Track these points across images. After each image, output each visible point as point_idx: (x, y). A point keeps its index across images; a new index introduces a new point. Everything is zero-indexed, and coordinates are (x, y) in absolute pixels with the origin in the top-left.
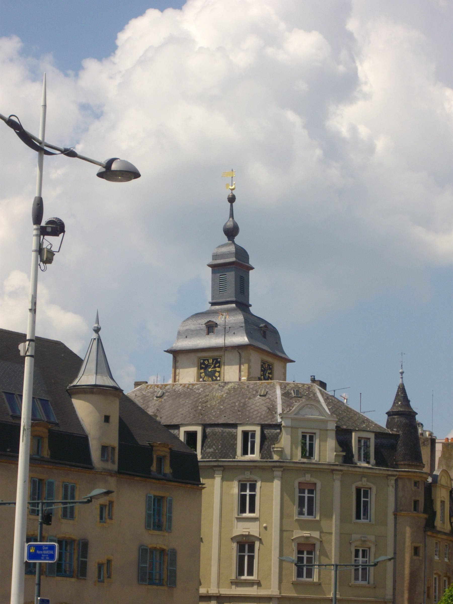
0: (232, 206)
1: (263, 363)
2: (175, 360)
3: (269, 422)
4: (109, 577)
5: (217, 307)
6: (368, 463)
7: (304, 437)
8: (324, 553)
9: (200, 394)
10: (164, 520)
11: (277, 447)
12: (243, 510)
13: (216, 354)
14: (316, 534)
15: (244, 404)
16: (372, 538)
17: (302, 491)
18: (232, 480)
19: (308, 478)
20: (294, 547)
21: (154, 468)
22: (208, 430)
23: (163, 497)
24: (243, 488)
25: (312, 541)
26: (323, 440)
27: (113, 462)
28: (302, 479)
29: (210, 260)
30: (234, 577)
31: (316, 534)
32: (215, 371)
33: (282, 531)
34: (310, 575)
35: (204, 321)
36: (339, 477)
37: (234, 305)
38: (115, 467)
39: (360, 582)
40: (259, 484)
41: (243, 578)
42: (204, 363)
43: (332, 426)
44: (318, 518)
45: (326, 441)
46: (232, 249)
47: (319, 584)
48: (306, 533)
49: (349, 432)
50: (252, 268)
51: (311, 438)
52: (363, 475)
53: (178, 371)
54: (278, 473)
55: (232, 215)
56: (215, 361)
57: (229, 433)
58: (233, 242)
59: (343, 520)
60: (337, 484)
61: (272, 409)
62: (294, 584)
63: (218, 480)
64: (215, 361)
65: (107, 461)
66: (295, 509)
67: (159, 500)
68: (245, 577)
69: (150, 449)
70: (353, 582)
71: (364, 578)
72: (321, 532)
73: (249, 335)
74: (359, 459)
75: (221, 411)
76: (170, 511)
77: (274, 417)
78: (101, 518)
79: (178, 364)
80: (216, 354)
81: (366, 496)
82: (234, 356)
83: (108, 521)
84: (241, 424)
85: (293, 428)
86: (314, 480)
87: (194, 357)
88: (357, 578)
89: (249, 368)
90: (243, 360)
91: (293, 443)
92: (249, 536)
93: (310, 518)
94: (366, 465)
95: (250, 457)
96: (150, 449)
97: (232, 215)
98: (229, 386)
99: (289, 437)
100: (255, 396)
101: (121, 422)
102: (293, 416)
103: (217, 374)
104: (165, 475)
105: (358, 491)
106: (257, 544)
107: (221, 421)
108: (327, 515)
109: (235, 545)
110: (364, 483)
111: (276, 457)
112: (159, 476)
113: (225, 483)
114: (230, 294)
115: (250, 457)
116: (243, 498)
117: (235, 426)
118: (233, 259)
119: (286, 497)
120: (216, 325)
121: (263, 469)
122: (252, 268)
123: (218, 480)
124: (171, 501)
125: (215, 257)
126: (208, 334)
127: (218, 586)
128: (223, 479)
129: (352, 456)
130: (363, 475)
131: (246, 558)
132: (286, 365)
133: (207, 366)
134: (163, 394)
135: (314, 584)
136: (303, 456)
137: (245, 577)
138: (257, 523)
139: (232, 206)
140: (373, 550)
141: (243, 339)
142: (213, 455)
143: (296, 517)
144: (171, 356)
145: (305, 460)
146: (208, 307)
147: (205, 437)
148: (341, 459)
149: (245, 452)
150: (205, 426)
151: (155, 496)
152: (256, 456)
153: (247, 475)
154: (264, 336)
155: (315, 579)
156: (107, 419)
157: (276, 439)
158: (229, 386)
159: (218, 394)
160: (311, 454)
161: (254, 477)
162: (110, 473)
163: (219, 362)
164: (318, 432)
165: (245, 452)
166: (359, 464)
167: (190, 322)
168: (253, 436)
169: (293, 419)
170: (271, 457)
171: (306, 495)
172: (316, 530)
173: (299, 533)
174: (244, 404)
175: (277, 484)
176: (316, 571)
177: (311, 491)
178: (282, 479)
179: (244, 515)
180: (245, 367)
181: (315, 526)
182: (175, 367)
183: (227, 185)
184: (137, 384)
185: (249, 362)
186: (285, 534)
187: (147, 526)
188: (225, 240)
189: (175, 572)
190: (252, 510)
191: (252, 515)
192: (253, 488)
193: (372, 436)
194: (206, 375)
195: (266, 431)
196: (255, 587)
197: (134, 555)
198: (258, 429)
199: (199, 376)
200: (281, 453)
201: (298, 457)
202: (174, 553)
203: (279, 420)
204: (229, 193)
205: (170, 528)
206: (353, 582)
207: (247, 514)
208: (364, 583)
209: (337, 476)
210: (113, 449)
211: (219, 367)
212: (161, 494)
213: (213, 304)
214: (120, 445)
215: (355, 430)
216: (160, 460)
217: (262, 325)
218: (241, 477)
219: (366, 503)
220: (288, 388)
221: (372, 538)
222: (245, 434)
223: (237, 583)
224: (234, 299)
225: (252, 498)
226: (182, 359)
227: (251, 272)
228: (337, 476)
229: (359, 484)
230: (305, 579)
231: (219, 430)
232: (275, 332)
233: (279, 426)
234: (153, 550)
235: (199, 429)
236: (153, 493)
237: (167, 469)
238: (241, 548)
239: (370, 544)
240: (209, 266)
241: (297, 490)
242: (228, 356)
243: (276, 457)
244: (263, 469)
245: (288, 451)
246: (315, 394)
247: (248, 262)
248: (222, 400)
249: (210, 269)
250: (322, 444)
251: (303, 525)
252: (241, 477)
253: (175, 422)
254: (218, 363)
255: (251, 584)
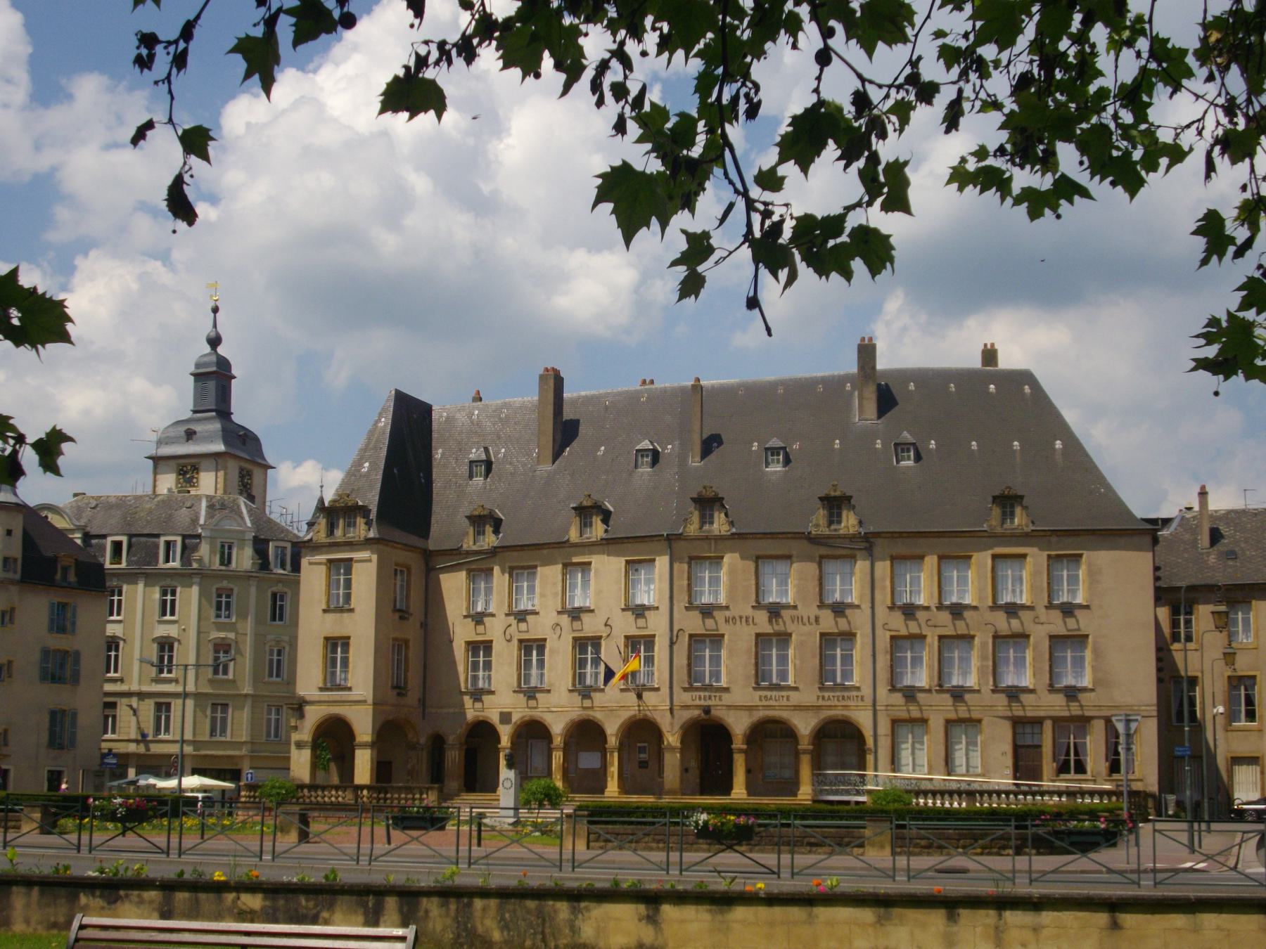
0: (215, 317)
1: (242, 469)
2: (155, 467)
3: (190, 532)
4: (10, 676)
5: (199, 415)
6: (284, 569)
7: (223, 546)
8: (239, 652)
9: (131, 506)
10: (68, 624)
11: (196, 555)
12: (164, 614)
13: (193, 461)
14: (232, 635)
15: (170, 515)
16: (286, 638)
17: (219, 596)
18: (154, 586)
19: (225, 584)
20: (211, 647)
21: (58, 576)
22: (134, 540)
23: (67, 604)
24: (164, 593)
25: (228, 642)
26: (241, 548)
27: (15, 572)
28: (219, 585)
29: (192, 369)
30: (154, 675)
31: (232, 635)
32: (193, 477)
33: (199, 633)
34: (225, 672)
35: (183, 429)
36: (255, 583)
37: (214, 414)
38: (18, 576)
39: (274, 679)
40: (178, 590)
41: (163, 675)
42: (182, 470)
43: (250, 535)
44: (234, 620)
45: (243, 549)
46: (214, 358)
47: (234, 681)
48: (222, 635)
49: (267, 541)
50: (235, 377)
51: (230, 548)
52: (279, 581)
53: (158, 477)
54: (196, 580)
55: (215, 326)
56: (1214, 330)
57: (153, 543)
58: (216, 351)
59: (258, 622)
60: (253, 590)
61: (195, 521)
62: (211, 682)
63: (141, 586)
64: (1214, 330)
65: (8, 571)
66: (213, 612)
67: (63, 607)
68: (165, 675)
69: (55, 560)
70: (267, 679)
71: (278, 676)
72: (237, 633)
73: (226, 443)
74: (276, 566)
75: (148, 522)
76: (74, 615)
77: (195, 527)
78: (3, 623)
79: (158, 470)
80: (193, 461)
81: (282, 600)
82: (211, 463)
83: (9, 625)
84: (164, 535)
85: (212, 539)
86: (231, 586)
87: (173, 463)
88: (271, 675)
89: (226, 474)
90: (219, 467)
91: (212, 552)
92: (168, 637)
93: (227, 620)
94: (282, 572)
95: (171, 564)
96: (55, 560)
97: (215, 326)
98: (160, 497)
99: (208, 546)
100: (181, 508)
101: (26, 535)
102: (211, 527)
103: (195, 480)
104: (70, 583)
105: (274, 595)
106: (176, 645)
107: (146, 532)
108: (243, 616)
109: (155, 646)
110: (279, 588)
111: (195, 565)
112: (65, 584)
113: (147, 589)
114: (211, 402)
115: (171, 564)
116: (164, 603)
117: (158, 536)
118: (214, 369)
119: (204, 602)
120: (195, 433)
121: (182, 575)
122: (235, 377)
123: (141, 586)
124: (75, 609)
125: (198, 366)
126: (188, 440)
127: (140, 683)
128: (146, 585)
129: (269, 563)
130: (279, 581)
131: (166, 657)
132: (266, 474)
133: (185, 473)
134: (97, 505)
135: (228, 681)
136: (222, 563)
137: (165, 675)
138: (177, 625)
139: (215, 317)
140: (287, 649)
141: (221, 447)
142: (137, 563)
143: (213, 620)
144: (151, 462)
145: (223, 568)
146: (188, 415)
147: (130, 546)
148: (257, 567)
149: (167, 560)
150: (131, 536)
151: (59, 604)
152: (175, 564)
153: (168, 582)
154: (244, 443)
155: (231, 676)
156: (9, 533)
157: (195, 548)
158: (160, 497)
159: (148, 506)
160: (229, 562)
161: (174, 583)
162: (12, 582)
163: (197, 469)
164: (235, 542)
165: (167, 560)
166: (275, 571)
167: (171, 429)
168: (175, 546)
169: (212, 530)
170: (191, 565)
171: (224, 599)
172: (231, 631)
173: (216, 635)
174: (170, 515)
175: (195, 590)
176: (174, 671)
177: (228, 596)
178: (200, 585)
179: (165, 618)
180: (221, 474)
181: (232, 627)
182: (155, 473)
183: (211, 296)
184: (75, 495)
185: (225, 468)
186: (202, 635)
187: (51, 630)
188: (207, 349)
189: (78, 671)
190: (172, 614)
191: (172, 618)
192: (174, 593)
193: (289, 545)
194: (185, 481)
195: (187, 541)
196: (174, 684)
197: (36, 656)
198: (179, 539)
199: (178, 482)
200: (200, 561)
201: (216, 565)
202: (77, 654)
203: (200, 531)
204: (212, 304)
205: (73, 631)
206: (267, 679)
207: (168, 617)
208: (279, 680)
209: (253, 583)
210: (15, 560)
211: (197, 473)
212: (65, 600)
213: (195, 412)
214: (24, 557)
215: (272, 540)
216: (65, 569)
217: (241, 433)
218: (163, 583)
219: (281, 607)
220: (214, 500)
221: (286, 638)
222: (168, 544)
223: (157, 681)
224: (214, 407)
225: (173, 602)
226: (162, 464)
227: (233, 381)
228: (253, 583)
229: (274, 589)
230: (221, 676)
231: (143, 539)
232: (256, 440)
233: (199, 536)
234: (57, 651)
235: (124, 539)
236: (56, 600)
237: (72, 578)
238: (162, 648)
239: (284, 644)
240: (192, 374)
241: (214, 595)
242: (204, 463)
243: (195, 565)
244: (182, 575)
245: (206, 560)
246: (239, 507)
247: (230, 371)
248: (150, 512)
249: (192, 378)
250: (240, 552)
251: (220, 627)
252: (163, 583)
253: (103, 532)
254: (196, 469)
255: (169, 681)
